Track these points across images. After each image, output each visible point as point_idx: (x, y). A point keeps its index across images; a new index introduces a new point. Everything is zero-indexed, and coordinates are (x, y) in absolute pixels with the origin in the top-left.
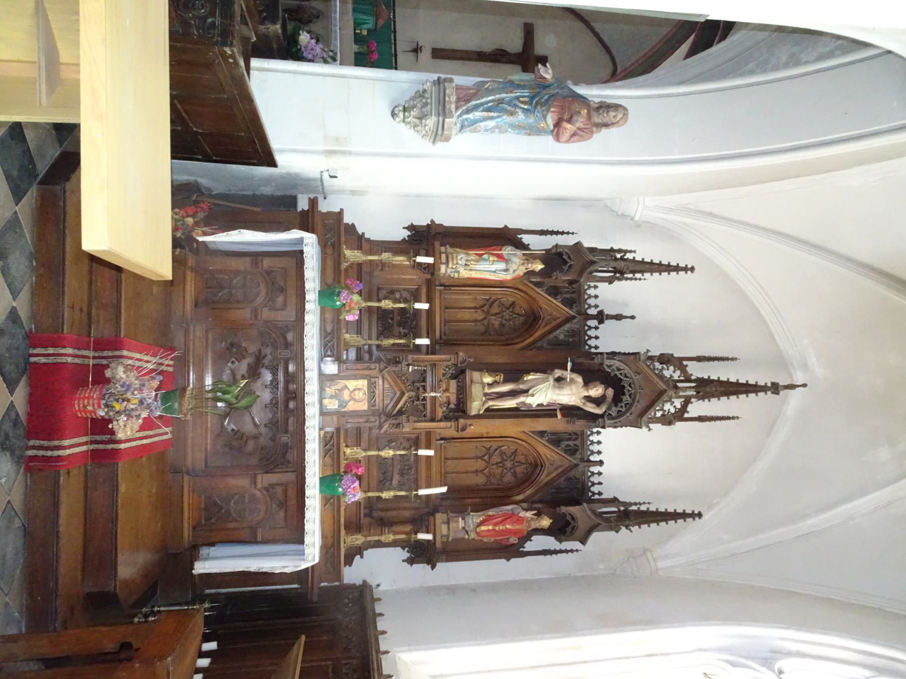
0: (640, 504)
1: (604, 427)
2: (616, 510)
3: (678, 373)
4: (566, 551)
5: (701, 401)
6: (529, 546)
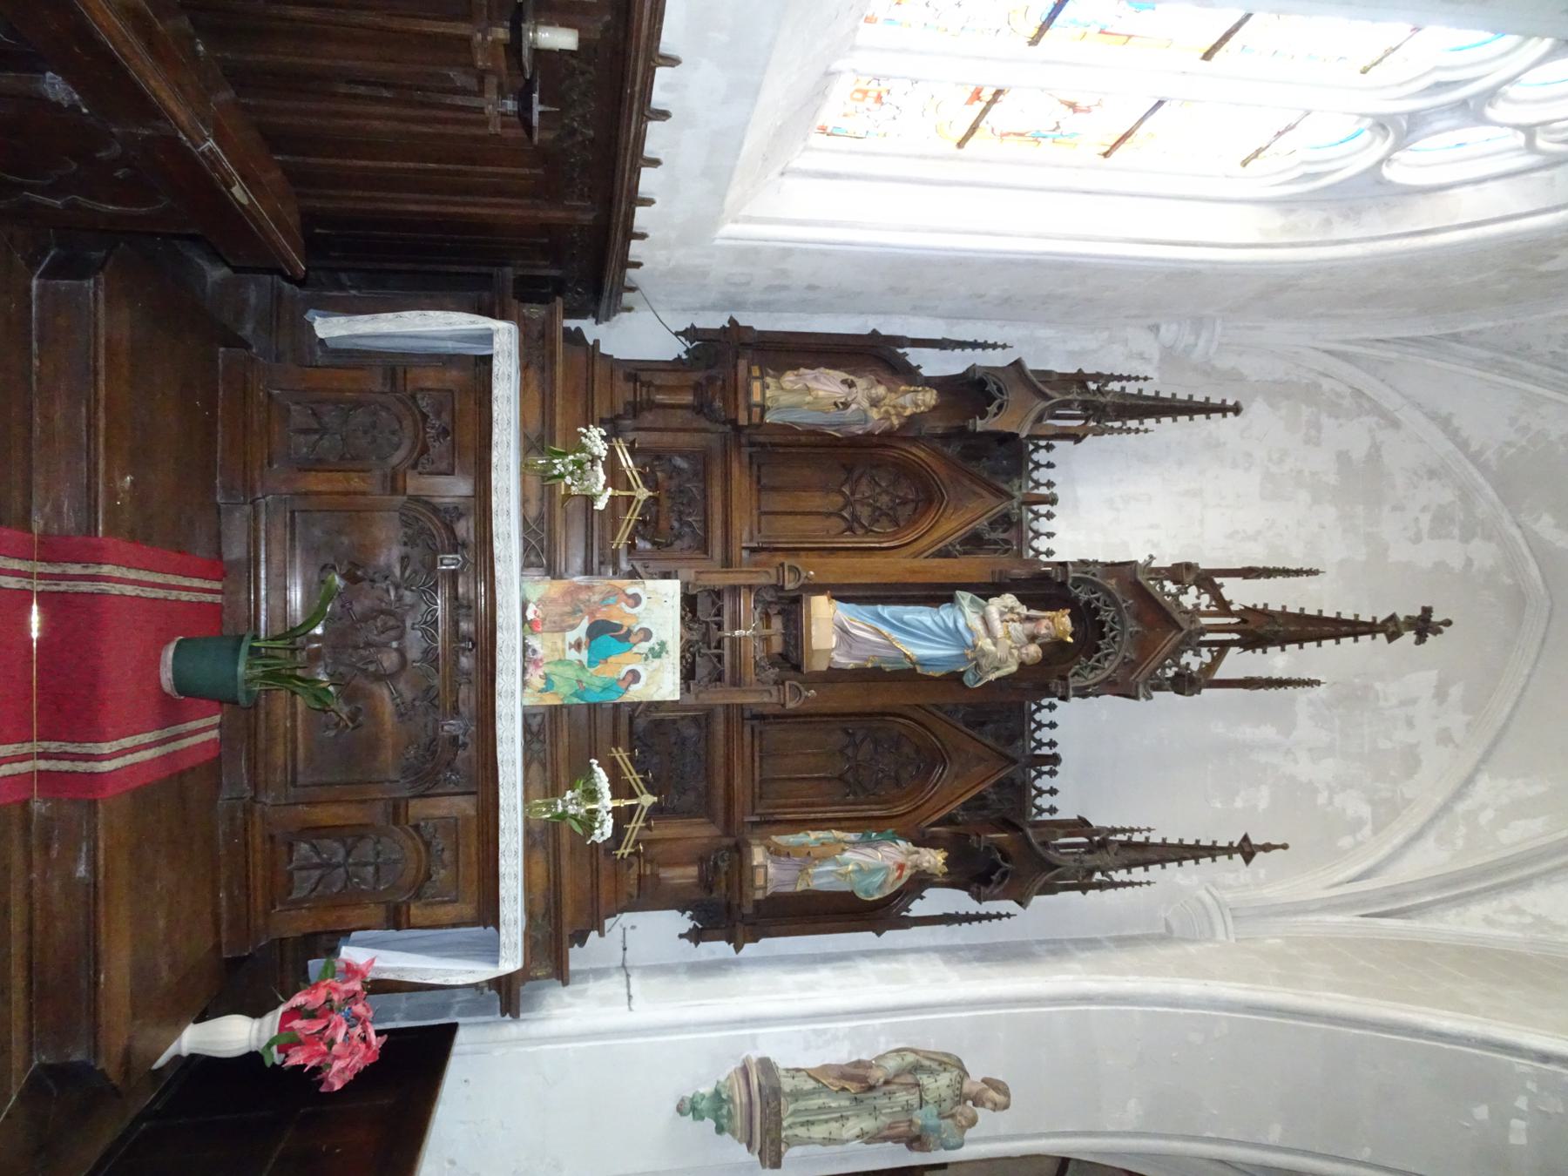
0: (1132, 830)
1: (1064, 698)
2: (1084, 840)
3: (1206, 599)
4: (989, 917)
5: (1250, 652)
6: (917, 908)
